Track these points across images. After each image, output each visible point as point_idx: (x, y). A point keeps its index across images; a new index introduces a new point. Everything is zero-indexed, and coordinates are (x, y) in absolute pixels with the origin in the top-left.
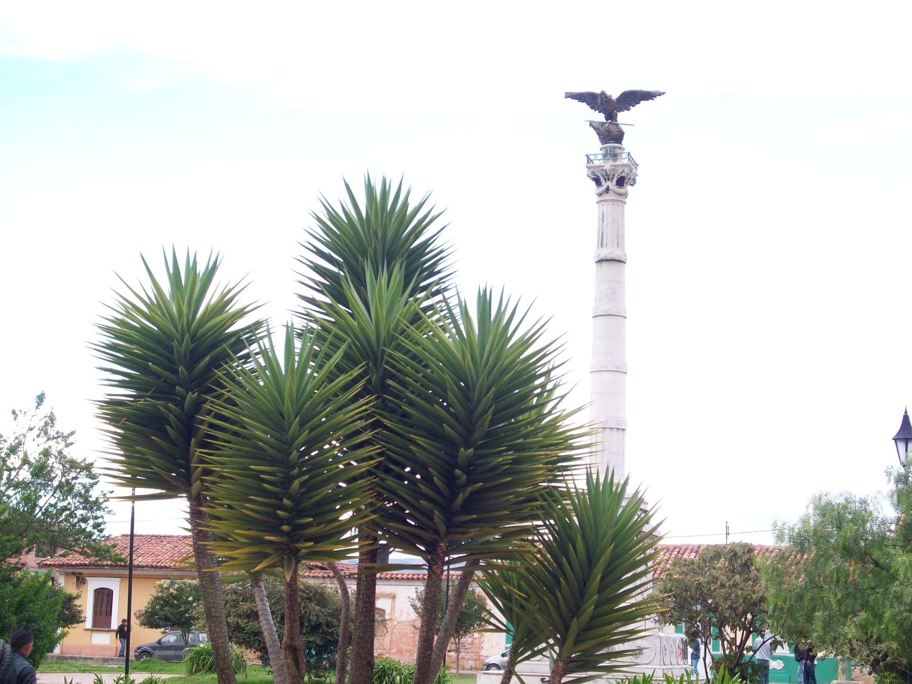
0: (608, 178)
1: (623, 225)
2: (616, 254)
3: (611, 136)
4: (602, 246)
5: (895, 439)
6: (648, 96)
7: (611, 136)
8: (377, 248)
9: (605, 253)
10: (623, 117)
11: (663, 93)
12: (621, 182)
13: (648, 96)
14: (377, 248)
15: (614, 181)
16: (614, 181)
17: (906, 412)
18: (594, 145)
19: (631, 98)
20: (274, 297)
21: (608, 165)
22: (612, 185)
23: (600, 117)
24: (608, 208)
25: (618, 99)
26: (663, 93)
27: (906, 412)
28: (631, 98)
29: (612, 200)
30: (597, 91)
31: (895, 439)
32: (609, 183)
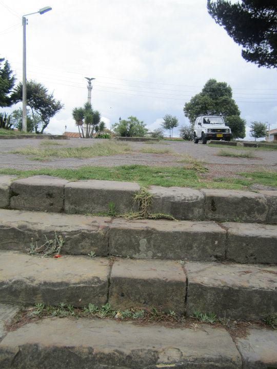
3: (90, 83)
7: (90, 83)
15: (90, 88)
16: (90, 88)
18: (88, 84)
19: (92, 79)
28: (92, 79)
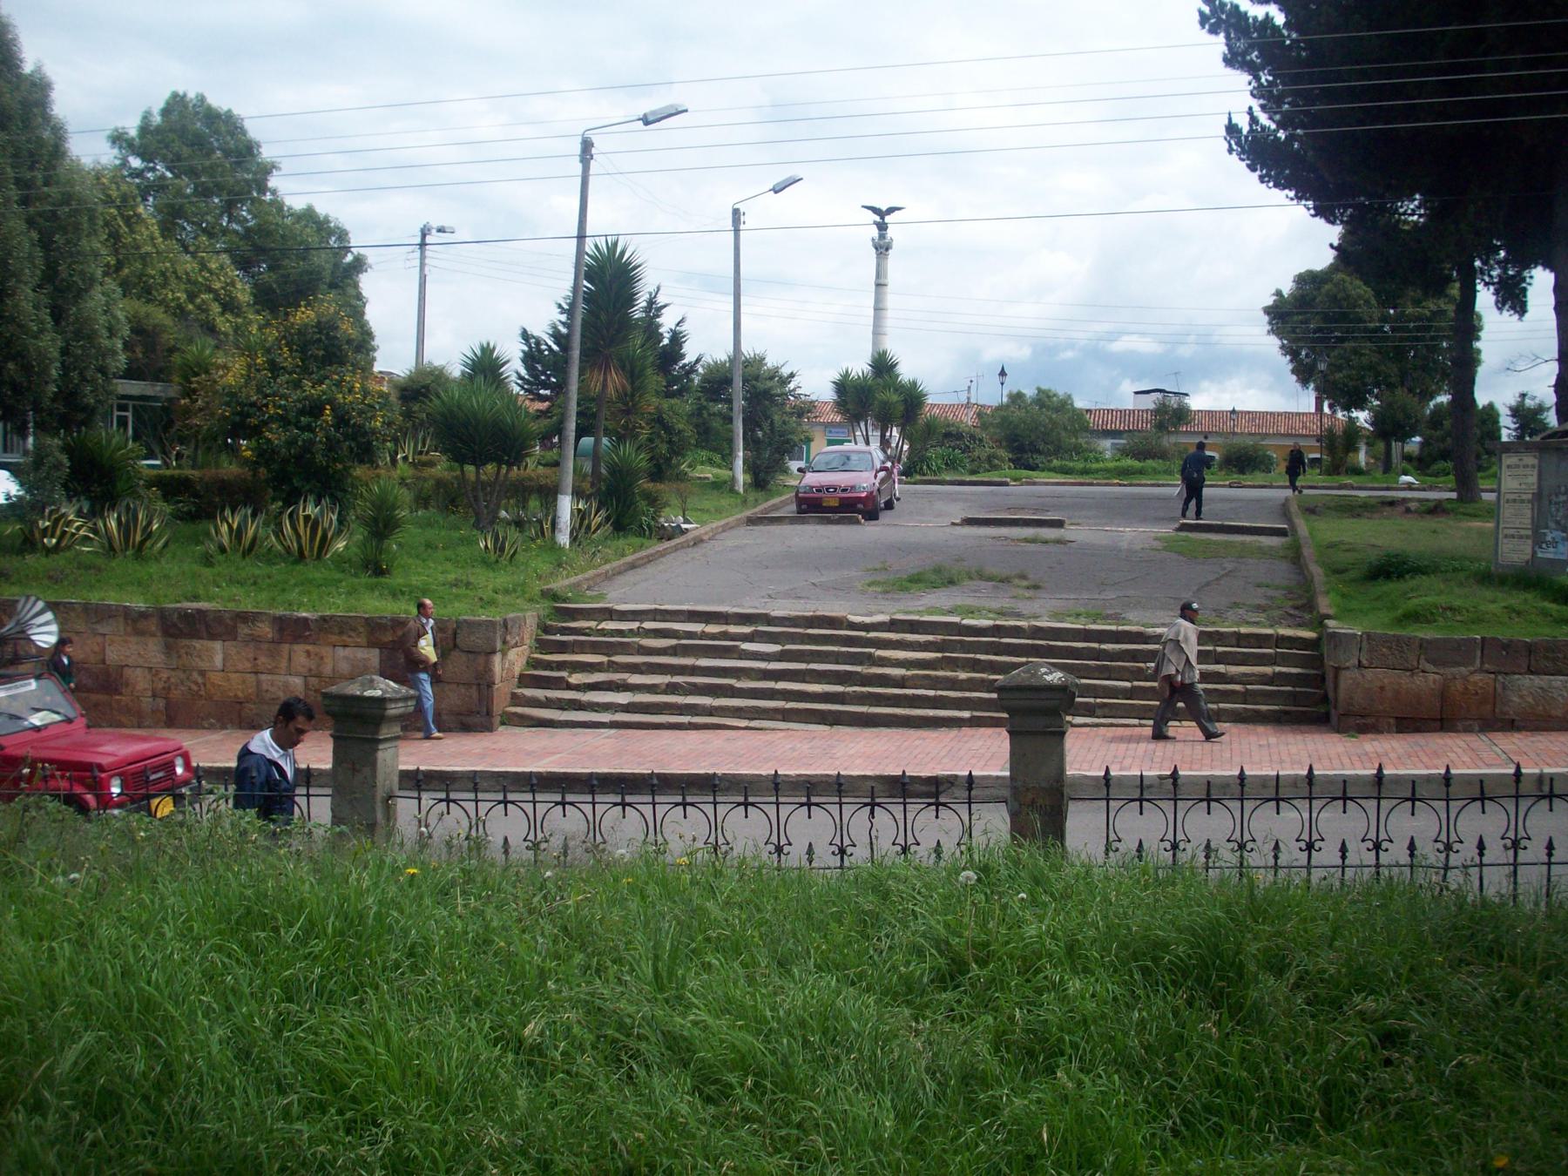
3: (882, 227)
7: (882, 227)
10: (887, 219)
15: (882, 248)
16: (882, 248)
18: (875, 232)
19: (891, 210)
23: (878, 219)
28: (891, 210)
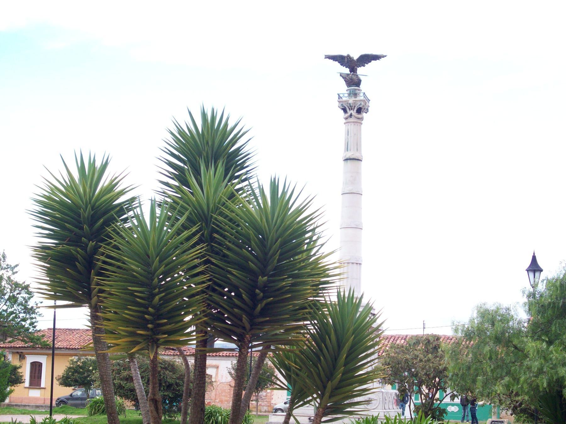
0: (351, 108)
1: (360, 138)
2: (356, 155)
3: (353, 82)
4: (347, 150)
5: (528, 270)
6: (376, 58)
7: (353, 82)
8: (208, 152)
9: (349, 155)
10: (360, 71)
11: (386, 56)
12: (359, 111)
13: (376, 58)
14: (208, 152)
15: (355, 110)
16: (355, 110)
17: (534, 254)
18: (343, 88)
19: (366, 59)
20: (144, 182)
21: (351, 101)
22: (354, 113)
23: (347, 71)
24: (351, 127)
25: (358, 59)
26: (386, 56)
27: (534, 254)
28: (366, 59)
29: (354, 122)
30: (345, 54)
31: (528, 270)
32: (352, 111)
